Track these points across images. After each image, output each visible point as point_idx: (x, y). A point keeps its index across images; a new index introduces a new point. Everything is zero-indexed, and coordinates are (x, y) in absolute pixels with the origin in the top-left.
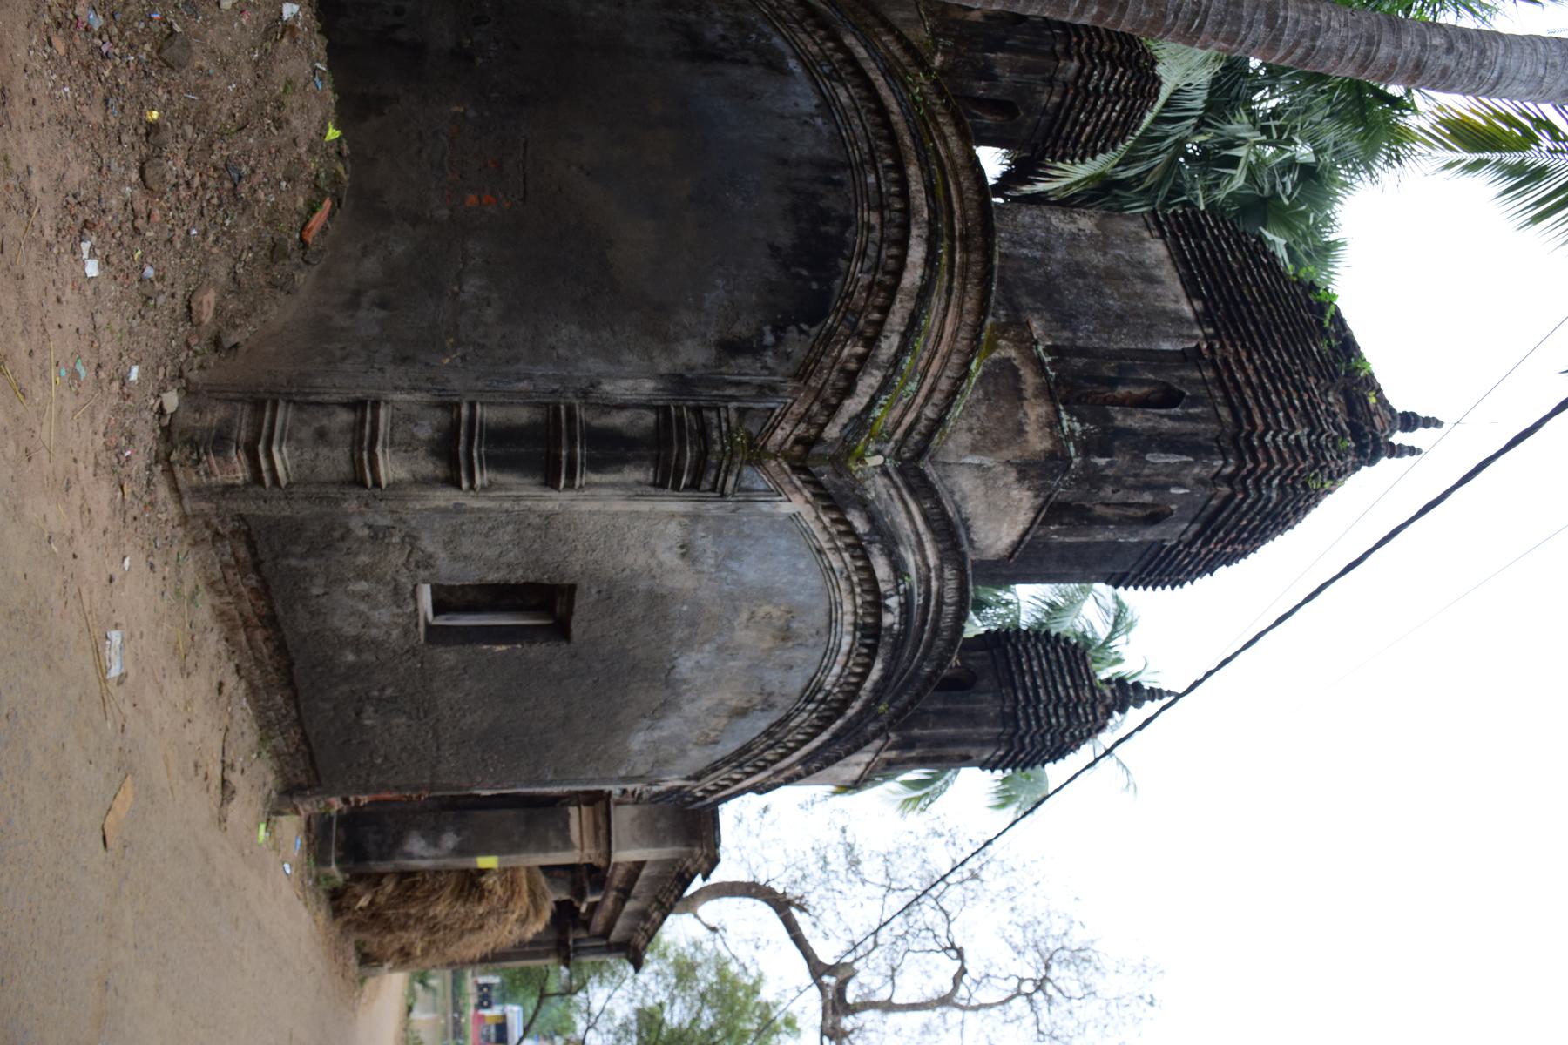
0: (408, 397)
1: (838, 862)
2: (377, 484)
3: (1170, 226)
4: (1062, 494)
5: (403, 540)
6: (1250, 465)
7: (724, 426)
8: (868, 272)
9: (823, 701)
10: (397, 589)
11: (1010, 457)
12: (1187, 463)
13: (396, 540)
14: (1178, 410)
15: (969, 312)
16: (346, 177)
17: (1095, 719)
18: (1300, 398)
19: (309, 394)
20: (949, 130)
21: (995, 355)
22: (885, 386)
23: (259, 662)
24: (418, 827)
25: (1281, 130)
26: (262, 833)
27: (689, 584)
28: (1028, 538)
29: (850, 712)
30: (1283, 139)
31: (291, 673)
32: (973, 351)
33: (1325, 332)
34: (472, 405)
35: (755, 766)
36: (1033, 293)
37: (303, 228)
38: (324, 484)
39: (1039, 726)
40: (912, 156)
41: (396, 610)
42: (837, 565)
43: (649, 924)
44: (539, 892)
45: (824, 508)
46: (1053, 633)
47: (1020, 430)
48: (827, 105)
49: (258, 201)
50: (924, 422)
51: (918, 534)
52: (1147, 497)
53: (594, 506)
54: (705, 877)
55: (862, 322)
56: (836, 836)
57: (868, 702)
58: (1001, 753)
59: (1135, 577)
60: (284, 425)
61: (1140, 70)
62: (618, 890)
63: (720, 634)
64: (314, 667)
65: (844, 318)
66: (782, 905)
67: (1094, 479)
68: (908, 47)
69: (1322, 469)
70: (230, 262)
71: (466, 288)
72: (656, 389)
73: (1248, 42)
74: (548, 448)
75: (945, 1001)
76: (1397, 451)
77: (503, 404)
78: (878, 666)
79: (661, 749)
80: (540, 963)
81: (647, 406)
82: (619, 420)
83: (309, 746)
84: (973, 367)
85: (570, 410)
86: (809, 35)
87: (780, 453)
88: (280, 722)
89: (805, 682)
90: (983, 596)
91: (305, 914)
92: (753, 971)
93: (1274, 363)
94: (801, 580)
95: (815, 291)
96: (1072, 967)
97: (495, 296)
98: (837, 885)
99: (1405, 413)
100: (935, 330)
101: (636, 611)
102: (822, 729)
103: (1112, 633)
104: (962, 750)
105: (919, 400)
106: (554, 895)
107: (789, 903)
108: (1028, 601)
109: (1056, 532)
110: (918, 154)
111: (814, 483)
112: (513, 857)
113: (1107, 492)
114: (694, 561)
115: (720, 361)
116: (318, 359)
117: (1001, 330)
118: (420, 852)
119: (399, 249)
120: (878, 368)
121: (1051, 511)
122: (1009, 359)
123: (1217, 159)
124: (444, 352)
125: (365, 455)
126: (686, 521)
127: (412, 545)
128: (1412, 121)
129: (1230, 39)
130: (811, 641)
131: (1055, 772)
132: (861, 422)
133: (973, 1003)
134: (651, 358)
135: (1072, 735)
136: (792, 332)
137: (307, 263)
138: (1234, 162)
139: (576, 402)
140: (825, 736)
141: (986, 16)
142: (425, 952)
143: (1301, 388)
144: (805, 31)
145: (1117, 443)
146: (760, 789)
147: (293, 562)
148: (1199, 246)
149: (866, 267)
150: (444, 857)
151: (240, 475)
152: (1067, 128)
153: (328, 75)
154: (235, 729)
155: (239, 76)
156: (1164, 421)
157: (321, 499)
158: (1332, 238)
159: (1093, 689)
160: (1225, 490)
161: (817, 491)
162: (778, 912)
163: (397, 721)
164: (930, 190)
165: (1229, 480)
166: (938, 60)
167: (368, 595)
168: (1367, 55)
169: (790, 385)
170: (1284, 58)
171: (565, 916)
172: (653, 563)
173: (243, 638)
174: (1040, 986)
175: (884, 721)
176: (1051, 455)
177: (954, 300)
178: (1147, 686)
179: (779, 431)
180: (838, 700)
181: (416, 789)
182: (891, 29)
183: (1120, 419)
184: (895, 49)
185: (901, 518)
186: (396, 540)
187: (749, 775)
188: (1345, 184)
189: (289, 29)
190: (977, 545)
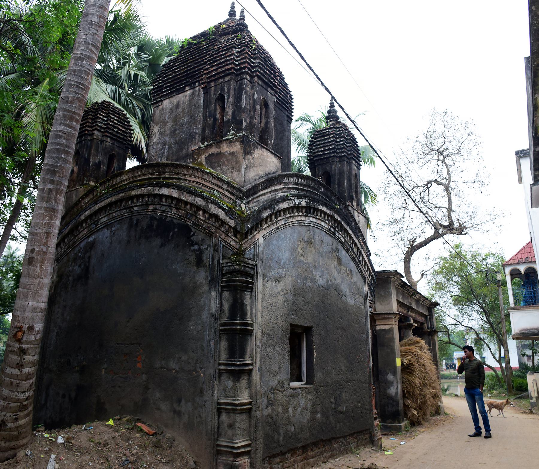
0: (216, 391)
1: (397, 227)
2: (250, 403)
3: (158, 98)
4: (256, 138)
5: (272, 393)
6: (247, 70)
7: (229, 264)
8: (171, 210)
9: (335, 229)
10: (292, 396)
11: (242, 158)
12: (245, 93)
13: (272, 396)
14: (226, 96)
15: (188, 172)
16: (129, 417)
17: (341, 127)
18: (222, 51)
19: (214, 431)
20: (119, 180)
21: (204, 163)
22: (215, 203)
23: (321, 454)
24: (386, 390)
25: (124, 58)
26: (389, 453)
27: (290, 279)
28: (273, 151)
29: (339, 219)
30: (128, 58)
31: (325, 440)
32: (202, 171)
33: (198, 43)
34: (220, 364)
35: (360, 256)
36: (181, 149)
37: (148, 434)
38: (250, 425)
39: (344, 148)
40: (128, 193)
41: (300, 396)
42: (283, 222)
43: (421, 299)
44: (410, 342)
45: (261, 227)
46: (309, 143)
47: (232, 154)
48: (107, 226)
49: (137, 453)
50: (229, 189)
51: (271, 192)
52: (258, 107)
53: (259, 315)
54: (403, 277)
55: (190, 212)
56: (386, 228)
57: (335, 212)
58: (354, 162)
59: (288, 113)
60: (225, 441)
61: (99, 108)
62: (408, 311)
63: (309, 268)
64: (323, 430)
65: (189, 219)
66: (413, 248)
67: (251, 126)
68: (86, 195)
69: (248, 44)
70: (161, 464)
71: (174, 367)
72: (215, 291)
73: (89, 67)
74: (237, 335)
75: (447, 188)
76: (242, 18)
77: (219, 352)
78: (321, 208)
79: (353, 291)
80: (437, 343)
81: (221, 294)
82: (226, 306)
83: (354, 433)
84: (208, 171)
85: (222, 325)
86: (80, 233)
87: (240, 242)
88: (345, 445)
89: (328, 236)
90: (296, 170)
91: (420, 436)
92: (438, 260)
93: (209, 60)
94: (288, 236)
95: (178, 230)
96: (433, 141)
97: (177, 356)
98: (405, 228)
99: (229, 15)
100: (194, 184)
101: (300, 300)
102: (345, 230)
103: (310, 122)
104: (353, 178)
105: (221, 190)
106: (411, 337)
107: (412, 246)
108: (298, 154)
109: (271, 141)
110: (127, 191)
111: (251, 230)
112: (396, 352)
113: (256, 122)
114: (281, 277)
115: (205, 266)
116: (201, 427)
117: (194, 160)
118: (395, 389)
119: (158, 395)
120: (208, 205)
121: (263, 142)
122: (206, 158)
123: (135, 81)
124: (199, 376)
125: (239, 408)
126: (265, 280)
127: (274, 390)
128: (123, 11)
129: (87, 74)
130: (312, 233)
131: (361, 143)
132: (228, 212)
133: (447, 178)
134: (203, 293)
135: (347, 136)
136: (194, 238)
137: (162, 433)
138: (136, 75)
139: (219, 322)
140: (348, 229)
141: (76, 165)
142: (434, 388)
143: (218, 51)
144: (79, 234)
145: (238, 118)
146: (369, 254)
147: (281, 438)
148: (165, 88)
149: (170, 211)
150: (397, 379)
151: (246, 460)
152: (120, 135)
153: (88, 424)
154: (348, 464)
155: (86, 461)
156: (230, 101)
157: (256, 426)
158: (165, 41)
159: (330, 128)
160: (256, 79)
161: (254, 229)
162: (415, 250)
163: (344, 397)
164: (141, 186)
165: (252, 77)
166: (92, 183)
167: (294, 408)
168: (96, 25)
169: (214, 239)
170: (96, 55)
171: (419, 332)
172: (282, 293)
173: (312, 460)
174: (441, 153)
175: (342, 206)
176: (242, 142)
177: (183, 177)
178: (329, 109)
179: (231, 243)
180: (334, 223)
181: (370, 390)
182: (79, 202)
183: (229, 116)
184: (86, 200)
185: (265, 197)
186: (272, 396)
187: (363, 258)
188: (145, 36)
189: (68, 440)
190: (275, 170)
